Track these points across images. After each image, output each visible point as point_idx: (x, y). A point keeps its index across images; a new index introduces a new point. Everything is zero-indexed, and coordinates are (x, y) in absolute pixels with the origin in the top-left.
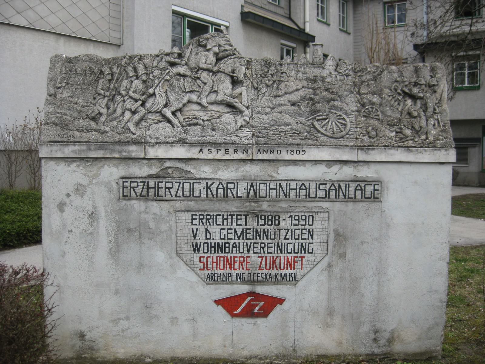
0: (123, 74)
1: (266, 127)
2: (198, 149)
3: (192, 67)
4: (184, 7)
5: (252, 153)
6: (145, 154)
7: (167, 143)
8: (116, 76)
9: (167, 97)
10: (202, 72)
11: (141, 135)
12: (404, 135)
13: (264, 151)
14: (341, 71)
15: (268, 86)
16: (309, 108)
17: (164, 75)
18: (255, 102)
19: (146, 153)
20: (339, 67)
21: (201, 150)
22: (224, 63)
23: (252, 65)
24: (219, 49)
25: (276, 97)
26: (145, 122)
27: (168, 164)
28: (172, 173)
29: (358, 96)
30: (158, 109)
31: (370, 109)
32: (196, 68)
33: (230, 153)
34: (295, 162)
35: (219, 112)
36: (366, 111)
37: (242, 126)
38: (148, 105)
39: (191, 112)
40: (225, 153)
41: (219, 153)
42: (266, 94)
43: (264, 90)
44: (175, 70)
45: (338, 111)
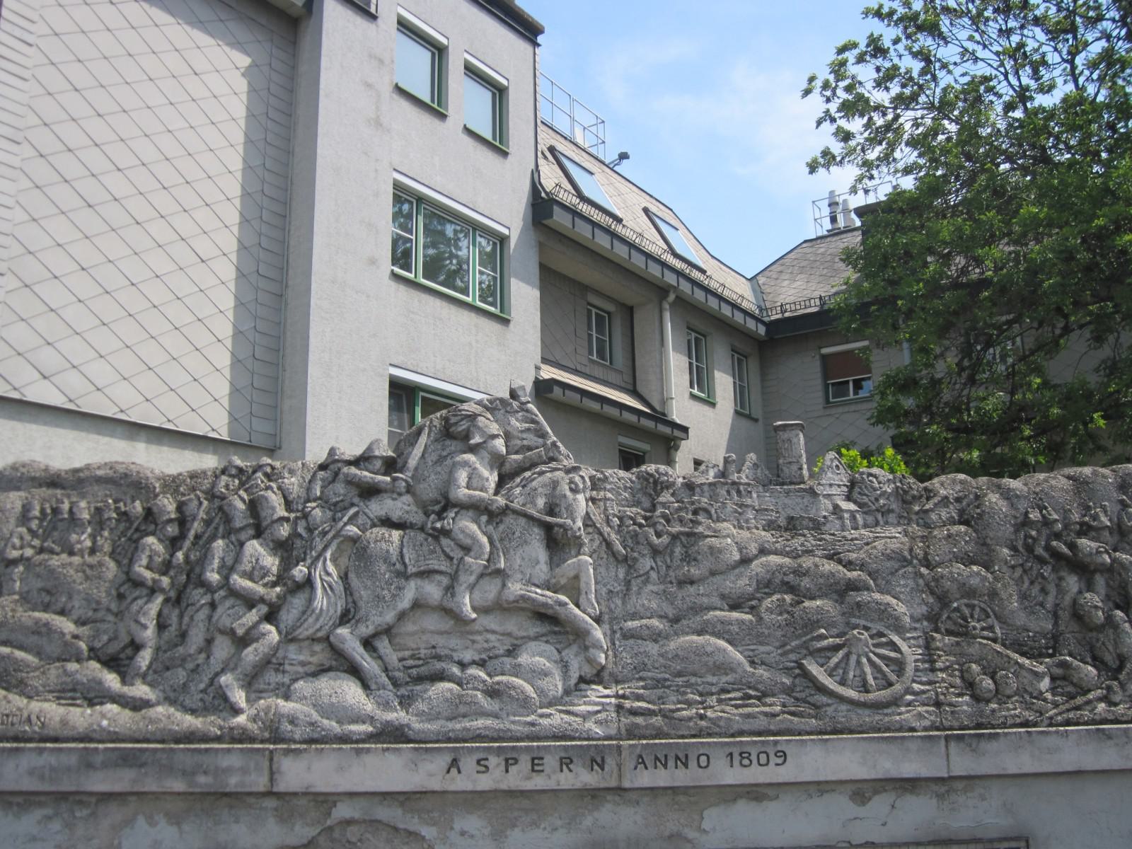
0: (217, 520)
1: (658, 681)
2: (443, 761)
3: (425, 497)
4: (415, 369)
5: (619, 766)
6: (272, 780)
7: (344, 739)
8: (196, 527)
9: (348, 589)
10: (457, 513)
11: (262, 714)
12: (1075, 685)
13: (657, 758)
14: (866, 499)
15: (655, 552)
16: (786, 616)
17: (341, 524)
18: (619, 602)
19: (276, 776)
20: (857, 489)
21: (454, 763)
22: (524, 487)
23: (605, 489)
24: (507, 446)
25: (681, 583)
26: (277, 670)
27: (343, 811)
28: (360, 840)
29: (923, 570)
30: (318, 630)
31: (967, 611)
32: (440, 503)
33: (547, 769)
34: (756, 793)
35: (509, 635)
36: (954, 615)
37: (582, 680)
38: (288, 616)
39: (424, 638)
40: (533, 770)
41: (513, 769)
42: (653, 575)
43: (646, 563)
44: (377, 508)
45: (872, 621)
